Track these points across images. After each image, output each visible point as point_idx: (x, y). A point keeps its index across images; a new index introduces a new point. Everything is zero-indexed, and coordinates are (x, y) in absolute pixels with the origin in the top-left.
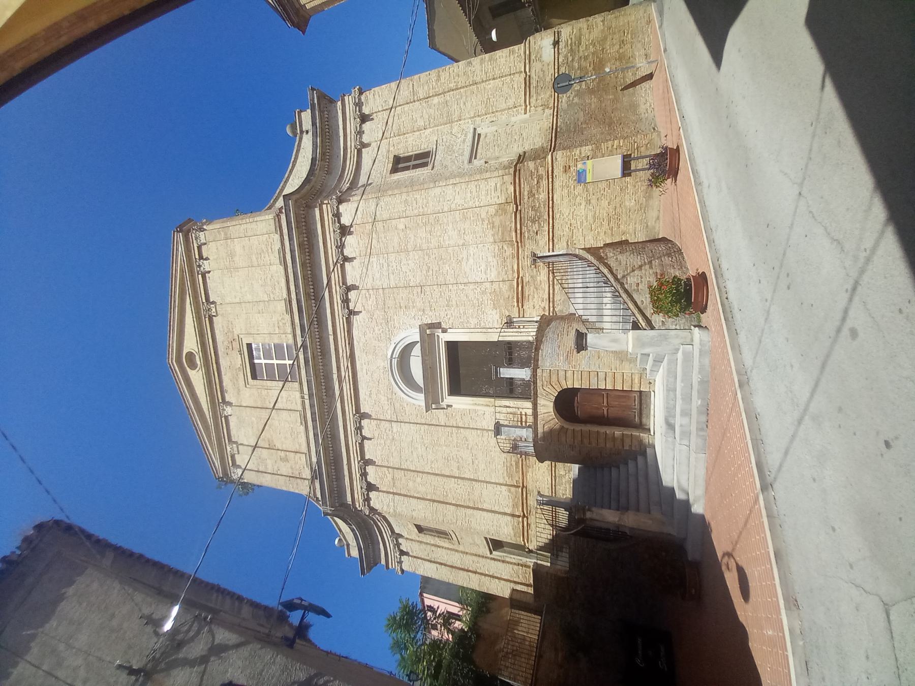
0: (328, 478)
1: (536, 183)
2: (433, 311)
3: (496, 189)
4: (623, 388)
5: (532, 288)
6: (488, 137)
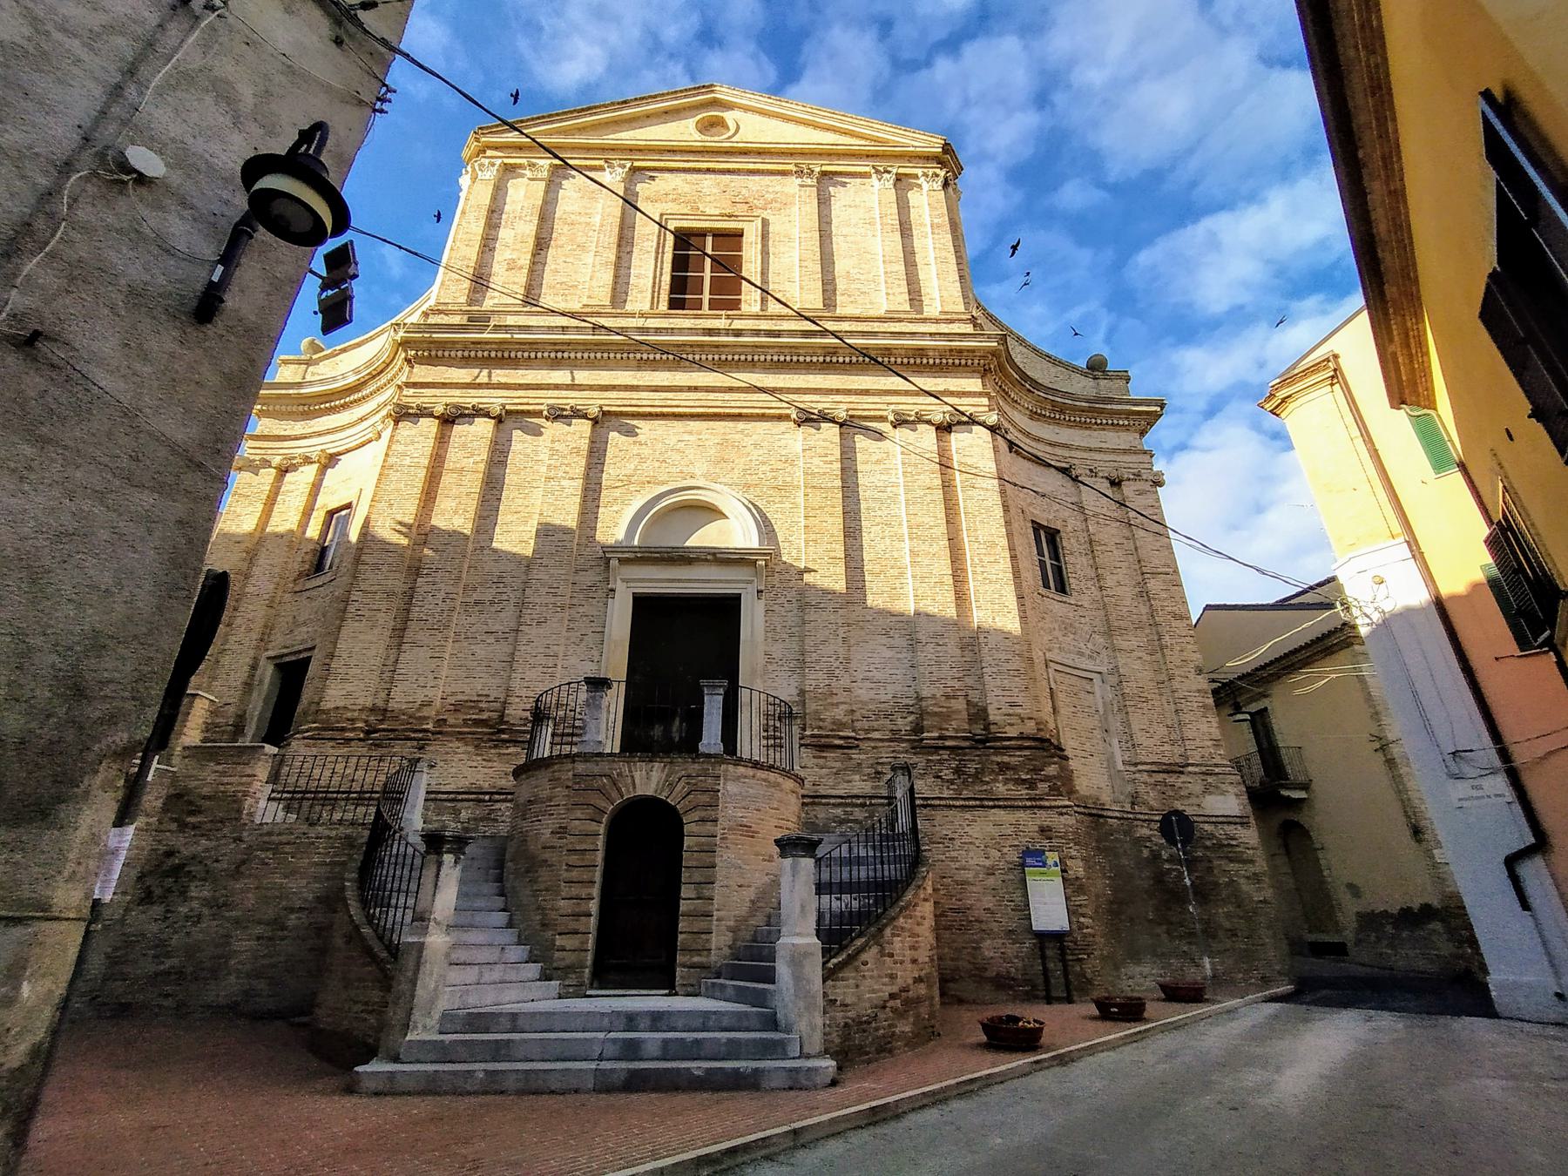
0: (473, 343)
1: (1023, 777)
2: (797, 577)
3: (1012, 705)
4: (681, 933)
5: (838, 765)
6: (1087, 696)
